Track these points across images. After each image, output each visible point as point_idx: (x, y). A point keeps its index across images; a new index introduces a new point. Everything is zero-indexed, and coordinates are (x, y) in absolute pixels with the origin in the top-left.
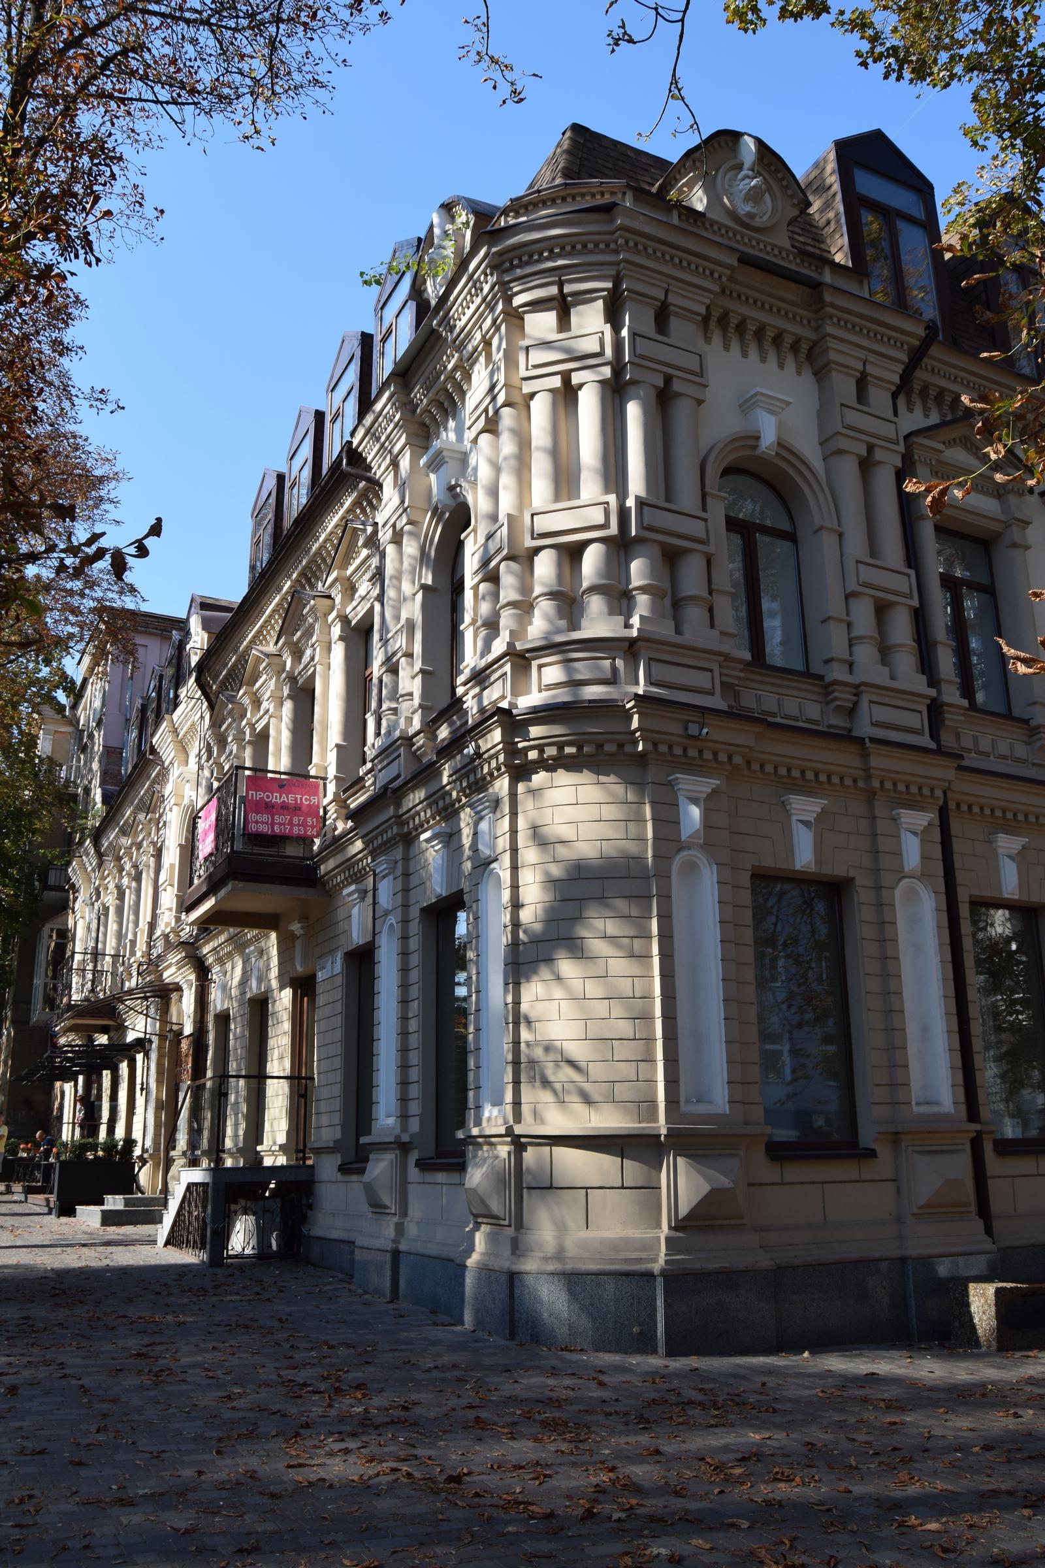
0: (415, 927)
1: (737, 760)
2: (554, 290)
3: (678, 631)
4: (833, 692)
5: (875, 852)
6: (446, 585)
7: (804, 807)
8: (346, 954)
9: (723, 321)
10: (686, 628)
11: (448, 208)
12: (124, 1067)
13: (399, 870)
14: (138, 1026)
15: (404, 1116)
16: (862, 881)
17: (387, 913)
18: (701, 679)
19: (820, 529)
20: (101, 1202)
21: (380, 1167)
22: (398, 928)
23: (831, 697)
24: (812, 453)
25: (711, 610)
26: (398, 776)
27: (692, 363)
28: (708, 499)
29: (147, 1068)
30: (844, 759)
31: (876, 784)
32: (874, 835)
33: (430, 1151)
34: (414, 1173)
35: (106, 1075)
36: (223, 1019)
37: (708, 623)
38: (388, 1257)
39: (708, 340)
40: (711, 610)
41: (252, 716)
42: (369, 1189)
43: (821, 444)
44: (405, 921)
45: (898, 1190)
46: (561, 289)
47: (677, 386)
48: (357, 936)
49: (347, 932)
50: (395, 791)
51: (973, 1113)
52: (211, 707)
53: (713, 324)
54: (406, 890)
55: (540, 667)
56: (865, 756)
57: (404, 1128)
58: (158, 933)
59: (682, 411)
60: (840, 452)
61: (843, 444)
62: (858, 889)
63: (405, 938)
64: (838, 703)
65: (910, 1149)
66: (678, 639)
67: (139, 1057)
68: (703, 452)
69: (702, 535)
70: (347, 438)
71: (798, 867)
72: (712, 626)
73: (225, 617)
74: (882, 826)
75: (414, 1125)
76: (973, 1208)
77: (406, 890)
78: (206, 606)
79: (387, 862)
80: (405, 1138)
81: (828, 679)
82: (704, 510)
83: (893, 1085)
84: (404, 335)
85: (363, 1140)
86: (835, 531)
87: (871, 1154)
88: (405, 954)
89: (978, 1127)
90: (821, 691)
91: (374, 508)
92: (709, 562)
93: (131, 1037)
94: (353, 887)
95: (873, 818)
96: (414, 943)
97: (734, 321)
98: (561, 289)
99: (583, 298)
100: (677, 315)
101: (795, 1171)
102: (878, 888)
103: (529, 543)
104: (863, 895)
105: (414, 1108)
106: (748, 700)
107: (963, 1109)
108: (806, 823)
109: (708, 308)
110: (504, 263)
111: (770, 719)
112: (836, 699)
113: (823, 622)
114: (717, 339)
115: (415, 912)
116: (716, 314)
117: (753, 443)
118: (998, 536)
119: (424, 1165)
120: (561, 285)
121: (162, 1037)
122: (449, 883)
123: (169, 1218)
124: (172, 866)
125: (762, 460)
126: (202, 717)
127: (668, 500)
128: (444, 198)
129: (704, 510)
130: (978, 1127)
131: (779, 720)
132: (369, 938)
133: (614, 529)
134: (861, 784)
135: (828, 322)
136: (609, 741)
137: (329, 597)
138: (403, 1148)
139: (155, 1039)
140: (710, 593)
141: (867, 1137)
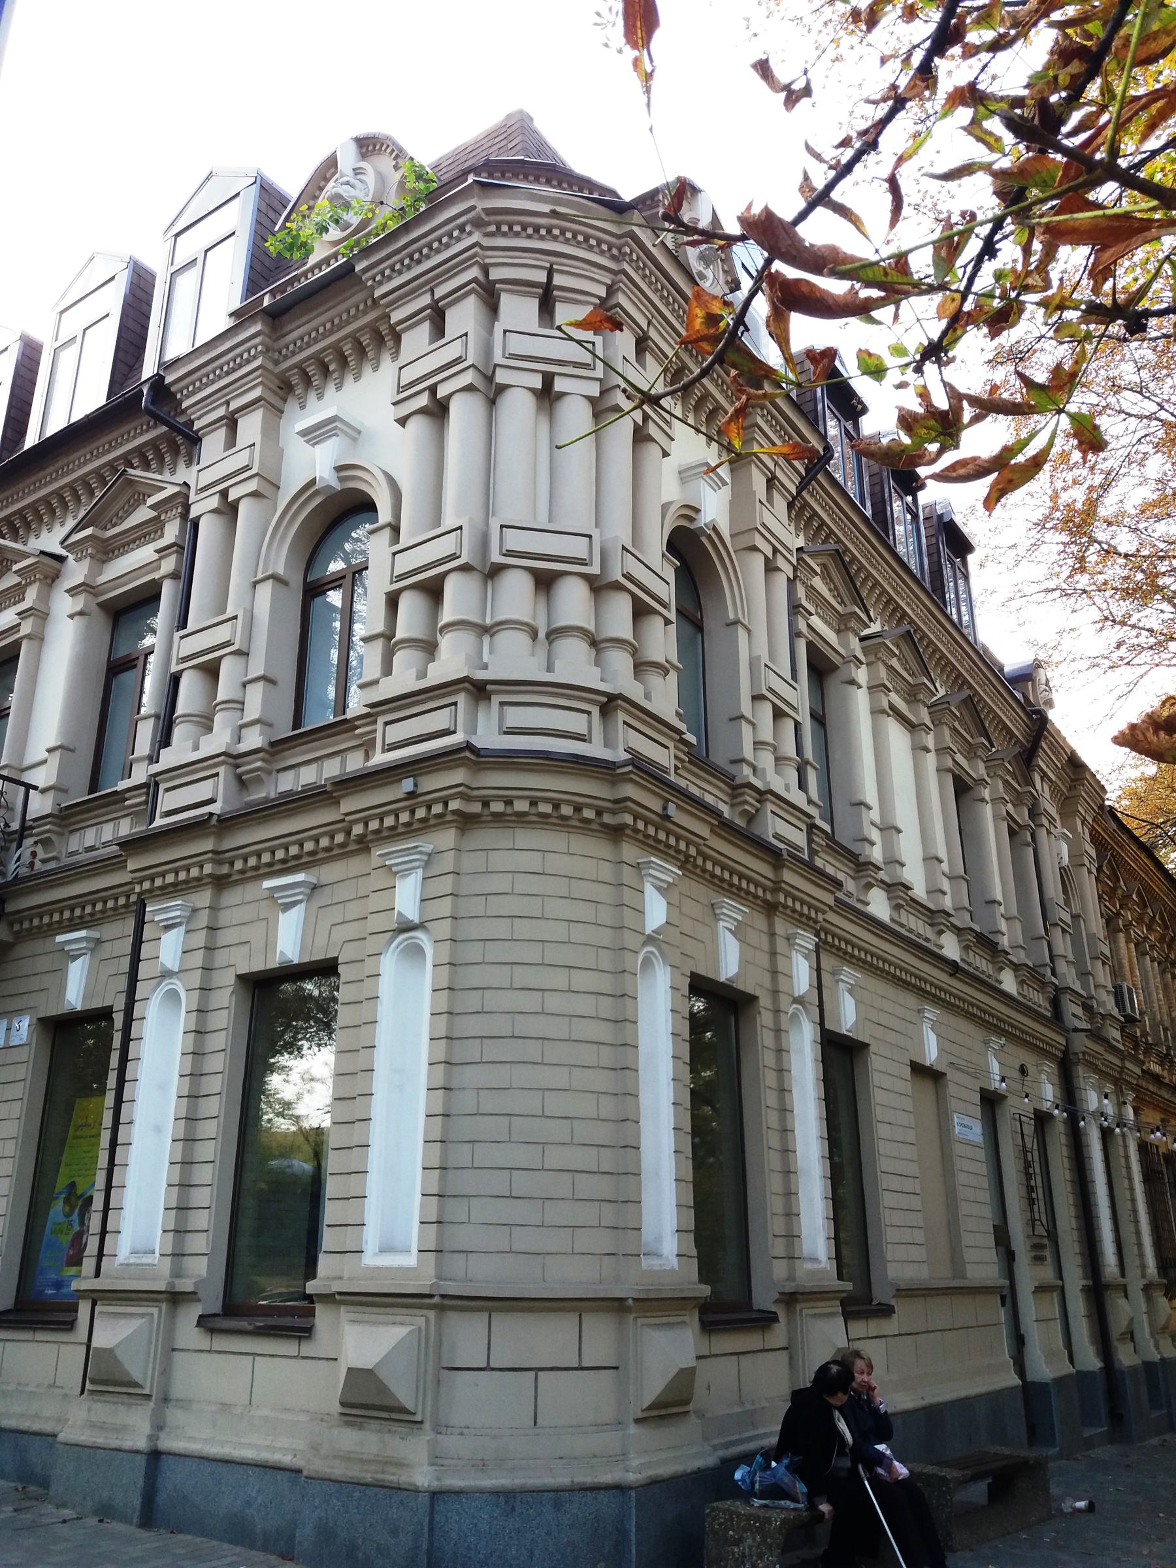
2: (542, 277)
4: (743, 794)
11: (368, 146)
13: (203, 919)
16: (765, 1001)
19: (736, 622)
23: (740, 799)
33: (216, 1307)
37: (374, 687)
38: (141, 1461)
45: (791, 1358)
57: (177, 1273)
61: (760, 542)
62: (761, 1010)
64: (746, 807)
65: (805, 1312)
71: (722, 979)
79: (182, 907)
81: (738, 781)
86: (527, 624)
90: (729, 791)
95: (772, 935)
99: (457, 296)
103: (496, 557)
110: (489, 224)
112: (746, 802)
113: (731, 720)
115: (227, 979)
117: (692, 514)
118: (834, 668)
120: (550, 273)
128: (363, 131)
135: (759, 411)
136: (588, 806)
138: (175, 1298)
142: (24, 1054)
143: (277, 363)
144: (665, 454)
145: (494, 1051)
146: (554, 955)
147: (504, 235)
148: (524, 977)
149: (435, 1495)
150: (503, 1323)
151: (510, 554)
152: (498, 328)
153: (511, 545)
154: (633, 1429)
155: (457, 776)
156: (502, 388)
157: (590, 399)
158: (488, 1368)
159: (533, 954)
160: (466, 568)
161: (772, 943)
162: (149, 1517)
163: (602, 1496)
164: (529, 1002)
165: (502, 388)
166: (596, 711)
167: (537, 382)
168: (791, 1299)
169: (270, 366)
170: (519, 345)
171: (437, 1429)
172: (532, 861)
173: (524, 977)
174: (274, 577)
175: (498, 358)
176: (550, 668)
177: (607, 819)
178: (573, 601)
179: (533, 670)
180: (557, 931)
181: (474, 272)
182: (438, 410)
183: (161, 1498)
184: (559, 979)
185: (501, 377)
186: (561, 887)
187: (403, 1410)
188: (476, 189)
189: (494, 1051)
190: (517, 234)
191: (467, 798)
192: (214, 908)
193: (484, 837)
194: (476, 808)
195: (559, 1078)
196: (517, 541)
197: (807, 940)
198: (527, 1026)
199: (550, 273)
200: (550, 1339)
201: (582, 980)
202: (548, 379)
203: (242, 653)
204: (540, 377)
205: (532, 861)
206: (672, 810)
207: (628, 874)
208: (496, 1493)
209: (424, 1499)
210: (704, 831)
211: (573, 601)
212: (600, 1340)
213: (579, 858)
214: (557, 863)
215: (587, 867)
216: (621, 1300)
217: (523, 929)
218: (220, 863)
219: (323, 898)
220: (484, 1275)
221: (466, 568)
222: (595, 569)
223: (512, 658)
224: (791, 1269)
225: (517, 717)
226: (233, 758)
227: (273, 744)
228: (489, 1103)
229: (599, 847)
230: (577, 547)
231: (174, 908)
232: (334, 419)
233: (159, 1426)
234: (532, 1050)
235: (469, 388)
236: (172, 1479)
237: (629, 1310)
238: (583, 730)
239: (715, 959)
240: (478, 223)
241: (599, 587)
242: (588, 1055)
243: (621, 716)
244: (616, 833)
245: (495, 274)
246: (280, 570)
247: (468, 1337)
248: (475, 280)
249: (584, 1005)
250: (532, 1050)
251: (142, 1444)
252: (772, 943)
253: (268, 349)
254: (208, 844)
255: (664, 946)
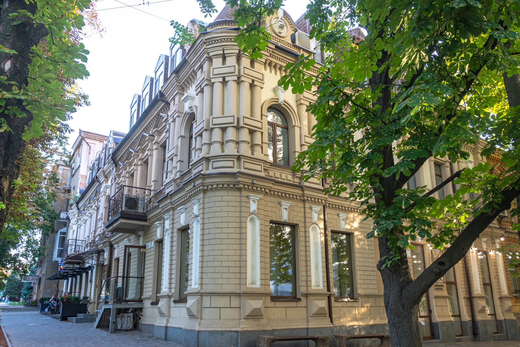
0: (175, 234)
1: (267, 190)
2: (221, 52)
3: (252, 154)
5: (305, 217)
6: (187, 136)
7: (286, 204)
8: (156, 241)
9: (270, 64)
10: (255, 153)
12: (84, 275)
14: (91, 262)
15: (170, 288)
16: (301, 225)
17: (167, 230)
18: (258, 168)
20: (76, 316)
21: (162, 303)
22: (170, 234)
24: (293, 104)
25: (262, 148)
26: (172, 191)
27: (260, 76)
28: (263, 116)
29: (93, 274)
30: (298, 192)
31: (306, 198)
32: (305, 213)
34: (172, 304)
35: (78, 277)
36: (118, 259)
38: (164, 328)
39: (265, 69)
40: (262, 148)
41: (129, 169)
42: (159, 308)
43: (296, 101)
44: (172, 233)
45: (307, 311)
46: (224, 52)
47: (256, 83)
48: (159, 236)
49: (156, 235)
50: (170, 195)
51: (329, 289)
52: (116, 166)
53: (267, 65)
54: (173, 224)
55: (213, 162)
56: (303, 190)
57: (170, 292)
58: (97, 234)
59: (257, 90)
60: (301, 104)
63: (172, 237)
66: (252, 156)
67: (90, 272)
68: (262, 103)
69: (260, 127)
70: (160, 89)
72: (262, 153)
73: (121, 139)
74: (307, 210)
75: (173, 291)
76: (328, 315)
77: (173, 224)
78: (115, 134)
80: (170, 294)
82: (262, 119)
83: (307, 281)
84: (178, 61)
85: (158, 295)
87: (300, 300)
88: (172, 242)
89: (329, 293)
91: (167, 111)
92: (262, 134)
93: (87, 265)
94: (158, 222)
95: (305, 208)
96: (175, 239)
97: (273, 65)
98: (224, 52)
99: (231, 55)
100: (257, 62)
101: (278, 304)
102: (305, 227)
103: (211, 126)
104: (301, 229)
105: (173, 286)
106: (271, 173)
107: (326, 288)
108: (286, 209)
109: (266, 60)
111: (277, 179)
114: (268, 68)
115: (175, 230)
116: (268, 62)
117: (277, 100)
119: (175, 302)
120: (224, 50)
121: (97, 265)
122: (185, 222)
123: (98, 320)
124: (102, 214)
125: (279, 105)
126: (113, 169)
127: (251, 116)
129: (262, 119)
130: (329, 293)
131: (280, 180)
132: (225, 88)
133: (235, 124)
134: (302, 198)
136: (231, 184)
137: (153, 136)
138: (170, 297)
139: (95, 266)
140: (262, 143)
141: (299, 296)
142: (152, 249)
143: (180, 83)
144: (262, 88)
145: (212, 242)
146: (224, 220)
147: (211, 44)
148: (217, 225)
149: (198, 332)
150: (214, 298)
151: (215, 125)
152: (212, 68)
153: (214, 123)
154: (243, 320)
155: (200, 181)
156: (213, 83)
157: (235, 81)
158: (210, 307)
159: (219, 220)
160: (205, 130)
161: (305, 210)
162: (166, 339)
163: (233, 333)
164: (218, 231)
165: (213, 83)
166: (235, 160)
167: (221, 80)
168: (306, 295)
169: (178, 84)
170: (216, 71)
171: (201, 319)
172: (219, 199)
173: (217, 225)
174: (181, 136)
175: (211, 76)
176: (223, 152)
177: (236, 186)
178: (231, 134)
179: (249, 154)
180: (225, 214)
181: (206, 55)
182: (202, 91)
183: (168, 336)
184: (225, 225)
185: (213, 81)
186: (226, 204)
187: (195, 316)
188: (202, 35)
189: (212, 242)
190: (214, 43)
191: (204, 186)
192: (173, 215)
193: (209, 194)
194: (206, 188)
195: (225, 247)
196: (216, 121)
197: (318, 208)
198: (218, 236)
199: (224, 50)
200: (224, 301)
201: (231, 225)
202: (224, 78)
203: (176, 155)
204: (222, 78)
205: (219, 199)
206: (255, 182)
207: (244, 199)
208: (210, 331)
209: (197, 332)
210: (270, 185)
211: (231, 134)
212: (235, 302)
213: (232, 197)
214: (224, 198)
215: (233, 198)
216: (240, 293)
217: (217, 214)
218: (172, 205)
219: (187, 211)
220: (210, 288)
221: (205, 130)
222: (235, 124)
223: (216, 150)
224: (307, 289)
225: (216, 165)
226: (174, 180)
227: (182, 176)
228: (211, 253)
229: (237, 194)
230: (230, 120)
231: (166, 216)
232: (187, 96)
233: (168, 321)
234: (219, 241)
235: (206, 85)
236: (170, 332)
237: (242, 296)
238: (232, 165)
239: (281, 216)
240: (204, 43)
241: (238, 128)
242: (233, 241)
243: (242, 160)
244: (240, 189)
245: (211, 54)
246: (183, 134)
247: (206, 301)
248: (206, 57)
249: (232, 230)
250: (219, 241)
251: (164, 325)
252: (305, 210)
253: (177, 80)
254: (169, 201)
255: (258, 215)
